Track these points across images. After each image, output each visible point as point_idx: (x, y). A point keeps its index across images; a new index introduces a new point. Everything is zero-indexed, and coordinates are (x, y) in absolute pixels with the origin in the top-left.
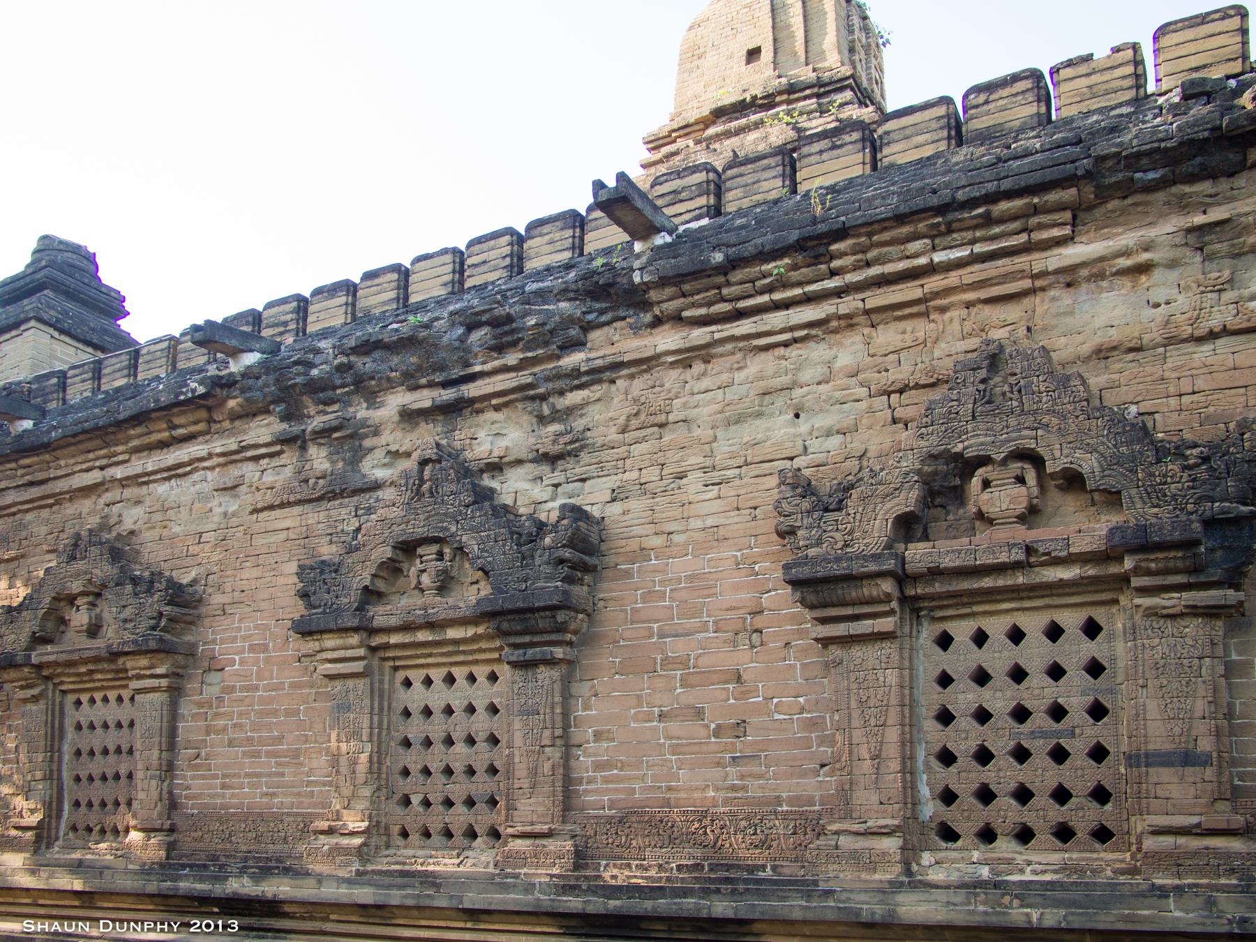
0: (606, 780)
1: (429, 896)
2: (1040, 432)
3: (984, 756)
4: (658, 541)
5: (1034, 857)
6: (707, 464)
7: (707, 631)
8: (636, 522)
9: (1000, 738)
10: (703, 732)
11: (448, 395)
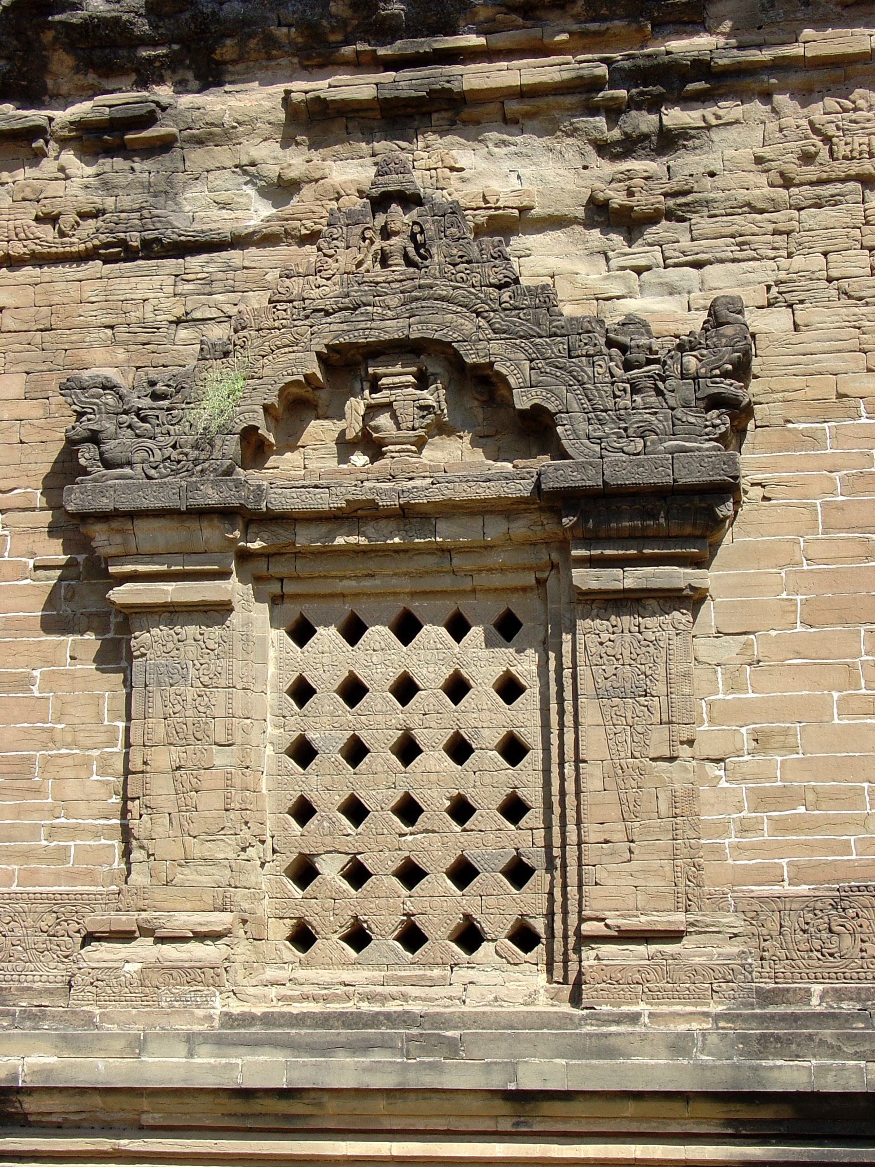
0: (781, 826)
1: (431, 1066)
8: (819, 346)
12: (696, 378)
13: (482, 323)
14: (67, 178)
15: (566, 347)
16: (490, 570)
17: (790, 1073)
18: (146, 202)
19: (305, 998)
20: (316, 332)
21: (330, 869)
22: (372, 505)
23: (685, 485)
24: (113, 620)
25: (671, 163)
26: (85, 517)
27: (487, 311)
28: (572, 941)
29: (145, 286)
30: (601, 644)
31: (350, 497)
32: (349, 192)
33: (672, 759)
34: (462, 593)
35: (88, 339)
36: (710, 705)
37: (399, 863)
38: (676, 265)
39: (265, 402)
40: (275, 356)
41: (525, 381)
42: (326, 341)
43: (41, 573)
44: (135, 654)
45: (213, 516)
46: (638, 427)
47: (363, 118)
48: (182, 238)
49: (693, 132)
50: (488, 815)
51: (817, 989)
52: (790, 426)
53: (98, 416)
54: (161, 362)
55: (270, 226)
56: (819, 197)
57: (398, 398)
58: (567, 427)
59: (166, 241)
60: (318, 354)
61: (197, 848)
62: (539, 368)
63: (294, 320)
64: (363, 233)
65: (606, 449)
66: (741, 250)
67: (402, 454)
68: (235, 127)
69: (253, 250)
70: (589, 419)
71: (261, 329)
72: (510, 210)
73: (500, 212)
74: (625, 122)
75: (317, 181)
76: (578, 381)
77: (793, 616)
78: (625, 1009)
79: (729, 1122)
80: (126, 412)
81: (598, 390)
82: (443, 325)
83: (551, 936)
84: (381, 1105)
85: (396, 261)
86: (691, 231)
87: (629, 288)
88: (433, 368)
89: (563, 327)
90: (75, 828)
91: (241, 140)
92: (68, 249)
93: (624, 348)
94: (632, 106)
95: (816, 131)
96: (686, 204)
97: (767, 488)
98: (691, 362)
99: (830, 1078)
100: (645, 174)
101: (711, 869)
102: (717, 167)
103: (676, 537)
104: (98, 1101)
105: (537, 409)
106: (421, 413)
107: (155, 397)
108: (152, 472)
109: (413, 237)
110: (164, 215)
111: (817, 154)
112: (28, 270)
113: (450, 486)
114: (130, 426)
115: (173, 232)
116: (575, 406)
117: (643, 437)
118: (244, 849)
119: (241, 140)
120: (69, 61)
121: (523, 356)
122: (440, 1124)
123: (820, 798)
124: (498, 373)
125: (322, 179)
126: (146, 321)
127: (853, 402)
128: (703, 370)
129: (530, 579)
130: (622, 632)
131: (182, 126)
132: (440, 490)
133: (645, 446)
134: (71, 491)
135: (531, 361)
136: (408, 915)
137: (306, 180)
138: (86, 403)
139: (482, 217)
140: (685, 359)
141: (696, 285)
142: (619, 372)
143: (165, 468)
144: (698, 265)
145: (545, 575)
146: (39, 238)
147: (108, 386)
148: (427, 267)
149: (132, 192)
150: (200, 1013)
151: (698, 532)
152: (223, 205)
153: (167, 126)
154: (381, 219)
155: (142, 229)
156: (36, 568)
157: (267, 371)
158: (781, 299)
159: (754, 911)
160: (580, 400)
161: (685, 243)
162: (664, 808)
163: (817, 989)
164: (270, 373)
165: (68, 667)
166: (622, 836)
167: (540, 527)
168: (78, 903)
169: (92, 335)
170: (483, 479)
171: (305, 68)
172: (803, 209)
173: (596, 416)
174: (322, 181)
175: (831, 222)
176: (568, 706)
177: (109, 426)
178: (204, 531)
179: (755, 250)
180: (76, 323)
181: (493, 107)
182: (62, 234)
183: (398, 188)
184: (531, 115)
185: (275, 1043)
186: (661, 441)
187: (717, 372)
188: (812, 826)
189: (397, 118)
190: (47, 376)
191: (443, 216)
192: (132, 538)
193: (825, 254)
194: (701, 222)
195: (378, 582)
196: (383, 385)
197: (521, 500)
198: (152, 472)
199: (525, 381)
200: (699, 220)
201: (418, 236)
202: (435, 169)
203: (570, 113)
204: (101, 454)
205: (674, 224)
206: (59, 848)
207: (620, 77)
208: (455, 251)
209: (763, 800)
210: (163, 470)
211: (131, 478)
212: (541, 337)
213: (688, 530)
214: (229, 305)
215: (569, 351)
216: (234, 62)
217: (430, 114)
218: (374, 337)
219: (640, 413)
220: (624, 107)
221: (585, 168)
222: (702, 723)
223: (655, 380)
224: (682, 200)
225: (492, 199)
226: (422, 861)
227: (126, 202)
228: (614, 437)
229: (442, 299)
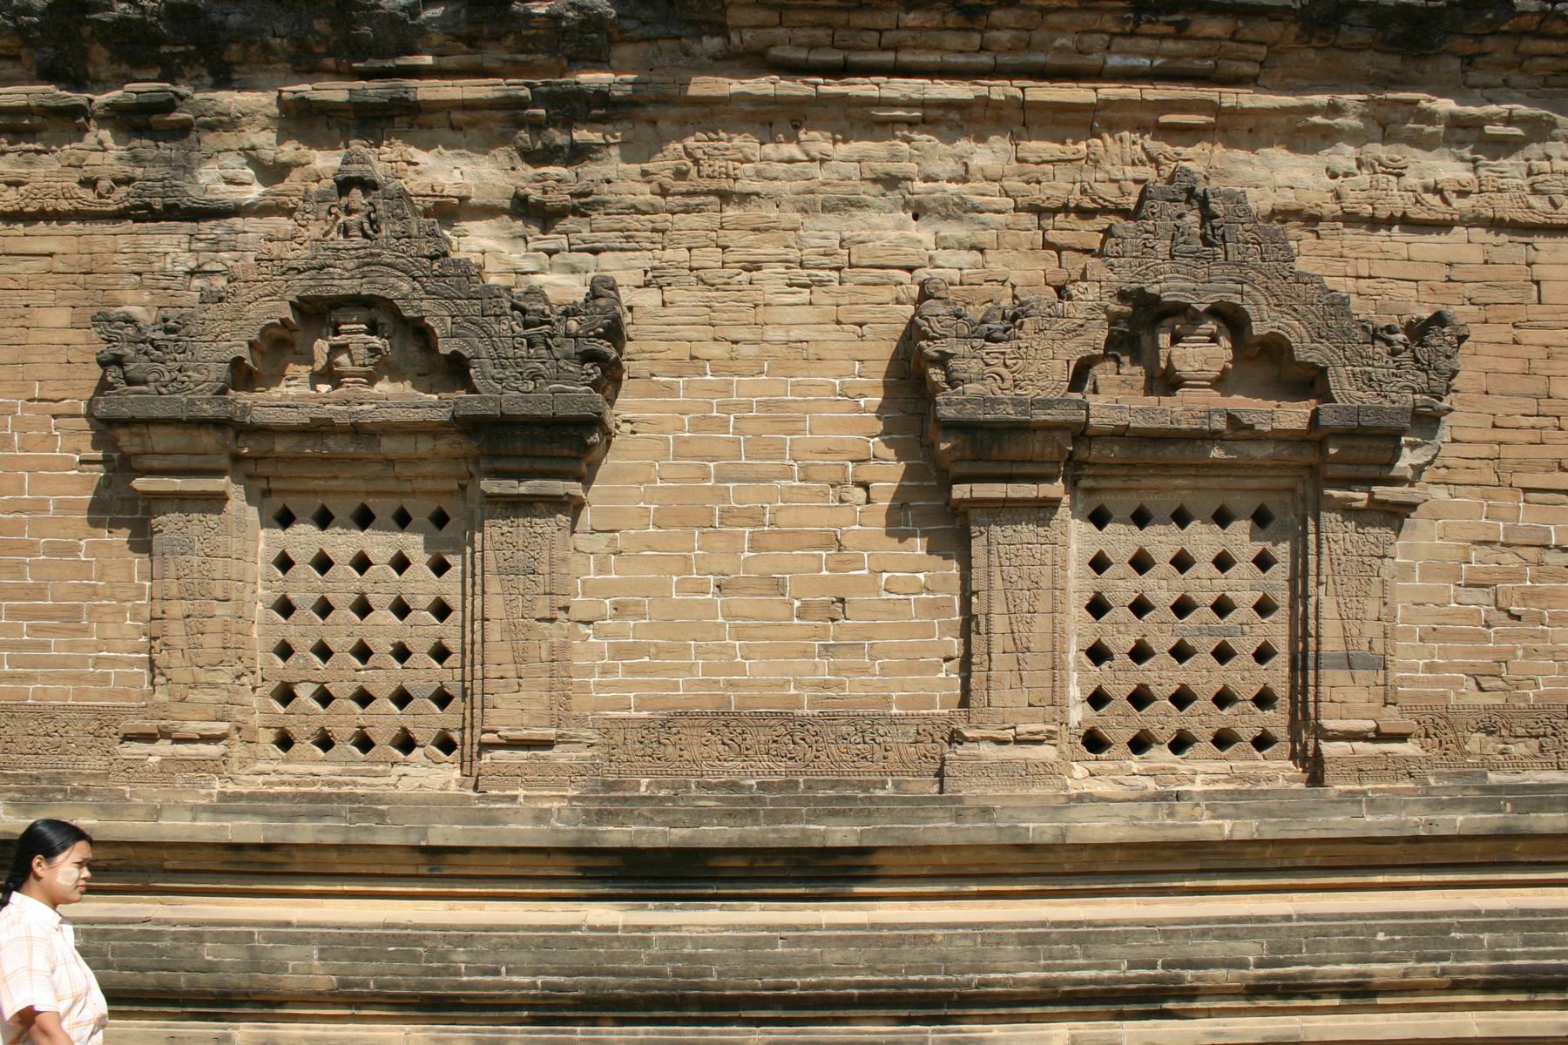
0: (630, 670)
1: (366, 829)
2: (1246, 288)
3: (1140, 653)
4: (718, 350)
5: (1199, 766)
6: (791, 257)
7: (792, 478)
9: (1161, 632)
10: (782, 611)
11: (373, 89)
12: (576, 337)
13: (417, 285)
14: (105, 150)
16: (425, 477)
17: (617, 835)
19: (283, 783)
21: (304, 693)
28: (476, 748)
33: (552, 620)
36: (583, 582)
37: (354, 690)
38: (578, 251)
43: (85, 466)
50: (421, 657)
51: (645, 781)
56: (687, 205)
60: (292, 303)
61: (203, 676)
69: (253, 219)
78: (508, 793)
79: (579, 869)
80: (143, 342)
82: (386, 286)
83: (463, 744)
84: (334, 856)
90: (114, 659)
93: (524, 311)
95: (689, 155)
98: (573, 325)
99: (644, 838)
101: (577, 700)
102: (612, 175)
104: (130, 851)
107: (168, 331)
111: (688, 171)
112: (73, 224)
114: (146, 353)
116: (484, 354)
118: (238, 677)
120: (106, 53)
122: (378, 870)
123: (660, 652)
127: (701, 363)
129: (454, 485)
136: (362, 727)
139: (429, 202)
141: (592, 267)
144: (595, 252)
147: (129, 320)
150: (203, 791)
152: (230, 182)
154: (344, 200)
156: (82, 462)
157: (251, 315)
159: (607, 729)
161: (586, 234)
162: (544, 655)
163: (645, 781)
166: (513, 674)
168: (114, 714)
171: (296, 72)
175: (695, 225)
176: (478, 580)
177: (129, 351)
181: (442, 116)
184: (471, 124)
185: (256, 813)
188: (652, 670)
189: (373, 121)
193: (689, 249)
194: (599, 218)
206: (102, 674)
207: (539, 98)
209: (619, 652)
213: (566, 452)
216: (239, 64)
217: (392, 117)
218: (334, 292)
222: (577, 595)
224: (583, 200)
225: (438, 189)
226: (371, 689)
227: (153, 173)
229: (388, 265)
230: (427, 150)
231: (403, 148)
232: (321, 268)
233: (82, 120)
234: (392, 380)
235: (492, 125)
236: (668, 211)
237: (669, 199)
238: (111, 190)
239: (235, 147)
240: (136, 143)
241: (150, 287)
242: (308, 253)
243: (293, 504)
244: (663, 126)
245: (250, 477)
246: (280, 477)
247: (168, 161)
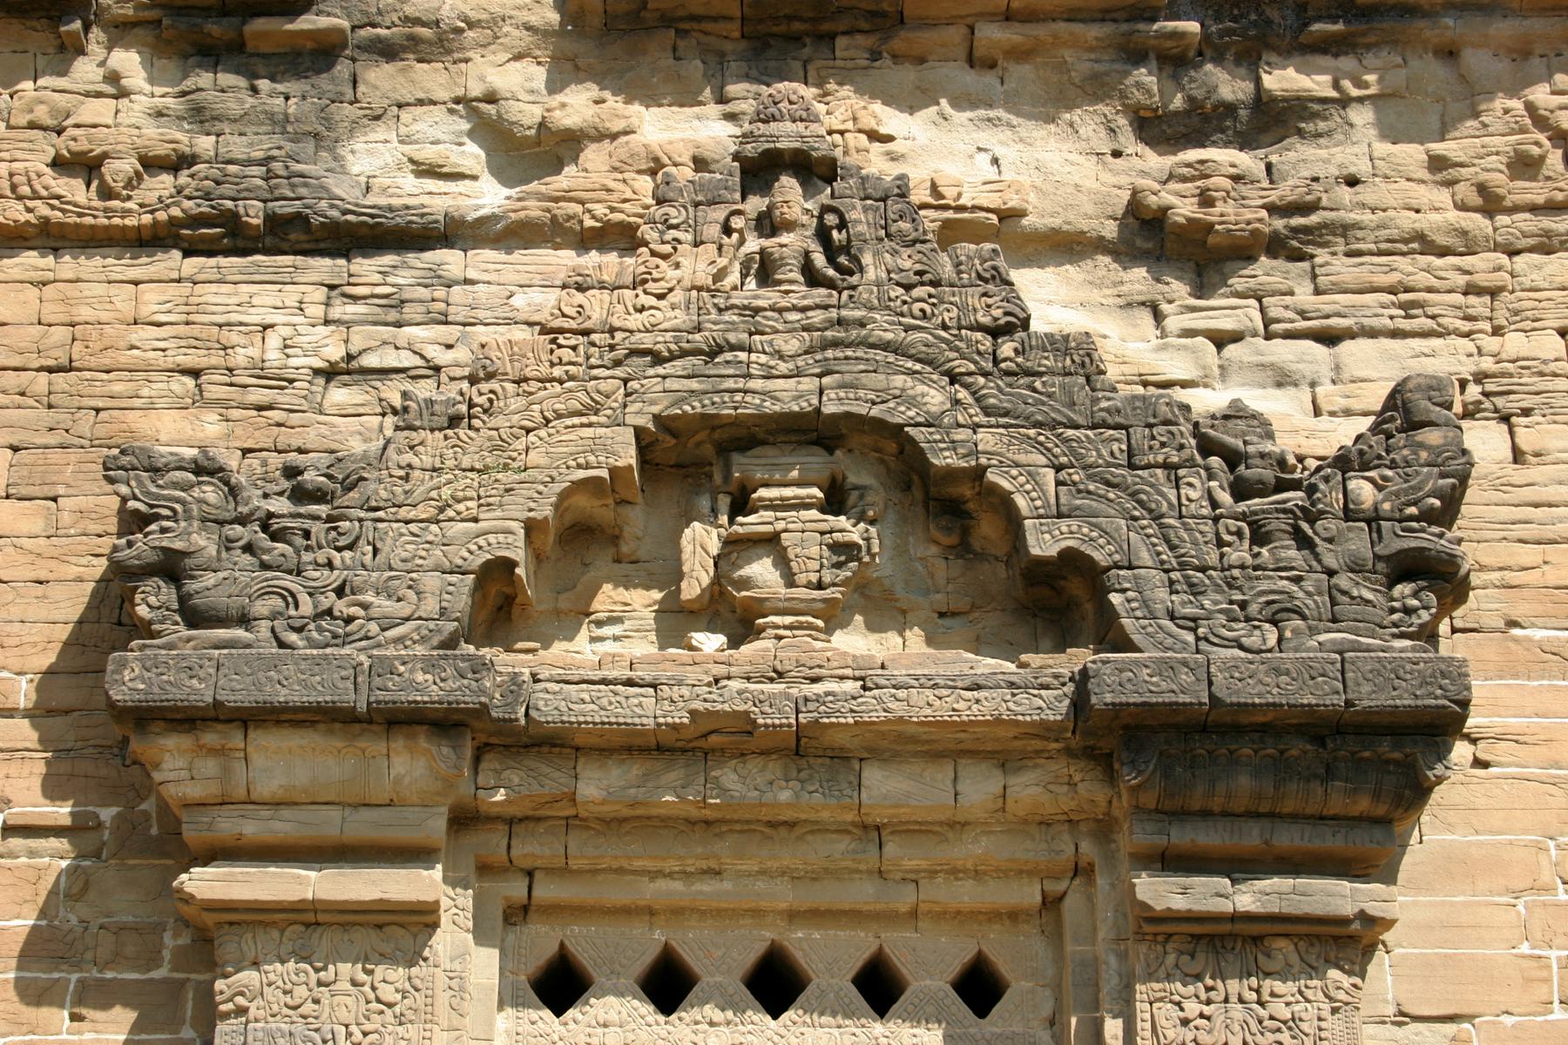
12: (1373, 519)
13: (963, 394)
14: (123, 94)
15: (1124, 447)
18: (279, 148)
20: (636, 391)
22: (744, 725)
23: (1368, 712)
24: (170, 942)
25: (1274, 158)
26: (148, 717)
27: (970, 374)
29: (270, 301)
30: (1185, 1022)
31: (698, 705)
32: (679, 160)
34: (888, 918)
35: (145, 392)
39: (531, 514)
40: (552, 431)
41: (1047, 505)
42: (656, 409)
44: (223, 1008)
45: (418, 728)
46: (1269, 603)
47: (706, 33)
48: (350, 217)
49: (1316, 107)
52: (1516, 632)
53: (183, 524)
54: (295, 443)
55: (524, 209)
56: (1547, 234)
57: (791, 526)
58: (1130, 594)
59: (316, 220)
60: (639, 432)
62: (1074, 483)
63: (592, 367)
64: (727, 220)
65: (1207, 640)
66: (1408, 317)
67: (796, 632)
68: (462, 31)
69: (488, 254)
70: (1171, 582)
71: (526, 380)
72: (983, 214)
73: (966, 215)
74: (1192, 80)
75: (614, 137)
76: (1150, 511)
77: (1544, 988)
80: (242, 520)
81: (1188, 529)
85: (791, 276)
86: (1314, 277)
87: (1204, 368)
88: (858, 476)
89: (1119, 411)
91: (470, 54)
92: (116, 221)
93: (1233, 459)
94: (1208, 53)
95: (1540, 122)
96: (1306, 230)
97: (1481, 744)
98: (1363, 490)
100: (1232, 171)
102: (1362, 168)
103: (1333, 818)
105: (1071, 559)
106: (835, 559)
108: (293, 637)
109: (823, 234)
110: (314, 174)
111: (1542, 158)
112: (31, 258)
113: (901, 694)
114: (249, 548)
115: (332, 206)
116: (1145, 557)
117: (1275, 623)
119: (470, 54)
121: (1043, 460)
124: (994, 489)
125: (626, 133)
126: (267, 364)
128: (1387, 506)
130: (1226, 1000)
131: (358, 18)
132: (879, 700)
133: (1280, 640)
134: (123, 664)
135: (1058, 469)
137: (593, 132)
138: (158, 497)
140: (1352, 485)
141: (1326, 373)
142: (1225, 497)
143: (320, 630)
144: (1329, 338)
145: (1061, 886)
146: (58, 197)
147: (205, 469)
148: (854, 288)
149: (250, 130)
151: (1381, 810)
153: (329, 15)
155: (269, 196)
158: (1487, 405)
160: (1154, 545)
161: (1304, 296)
164: (543, 461)
165: (65, 1036)
167: (1066, 788)
169: (154, 386)
170: (967, 683)
172: (1518, 252)
173: (1186, 577)
174: (623, 139)
177: (204, 542)
178: (395, 760)
179: (1433, 317)
180: (122, 360)
181: (956, 34)
182: (106, 193)
183: (797, 145)
184: (1019, 54)
186: (1313, 631)
187: (1413, 510)
190: (56, 456)
191: (884, 200)
192: (239, 767)
194: (1336, 265)
195: (727, 885)
196: (761, 499)
197: (1044, 730)
198: (293, 637)
199: (1047, 505)
200: (1328, 258)
201: (835, 233)
202: (842, 133)
203: (1093, 56)
204: (183, 599)
205: (1280, 263)
208: (908, 264)
210: (315, 634)
211: (248, 646)
212: (1077, 427)
213: (1363, 805)
214: (437, 347)
215: (1130, 454)
217: (831, 37)
218: (752, 405)
219: (1270, 578)
220: (1191, 54)
221: (1117, 154)
223: (1296, 518)
224: (1297, 221)
227: (237, 146)
228: (1222, 619)
230: (912, 110)
231: (857, 102)
232: (713, 352)
233: (77, 25)
234: (872, 627)
235: (1068, 55)
236: (1497, 248)
237: (1503, 220)
238: (133, 182)
239: (442, 94)
240: (204, 79)
241: (223, 404)
242: (680, 318)
243: (587, 943)
244: (1476, 60)
245: (485, 869)
246: (563, 871)
247: (280, 123)
